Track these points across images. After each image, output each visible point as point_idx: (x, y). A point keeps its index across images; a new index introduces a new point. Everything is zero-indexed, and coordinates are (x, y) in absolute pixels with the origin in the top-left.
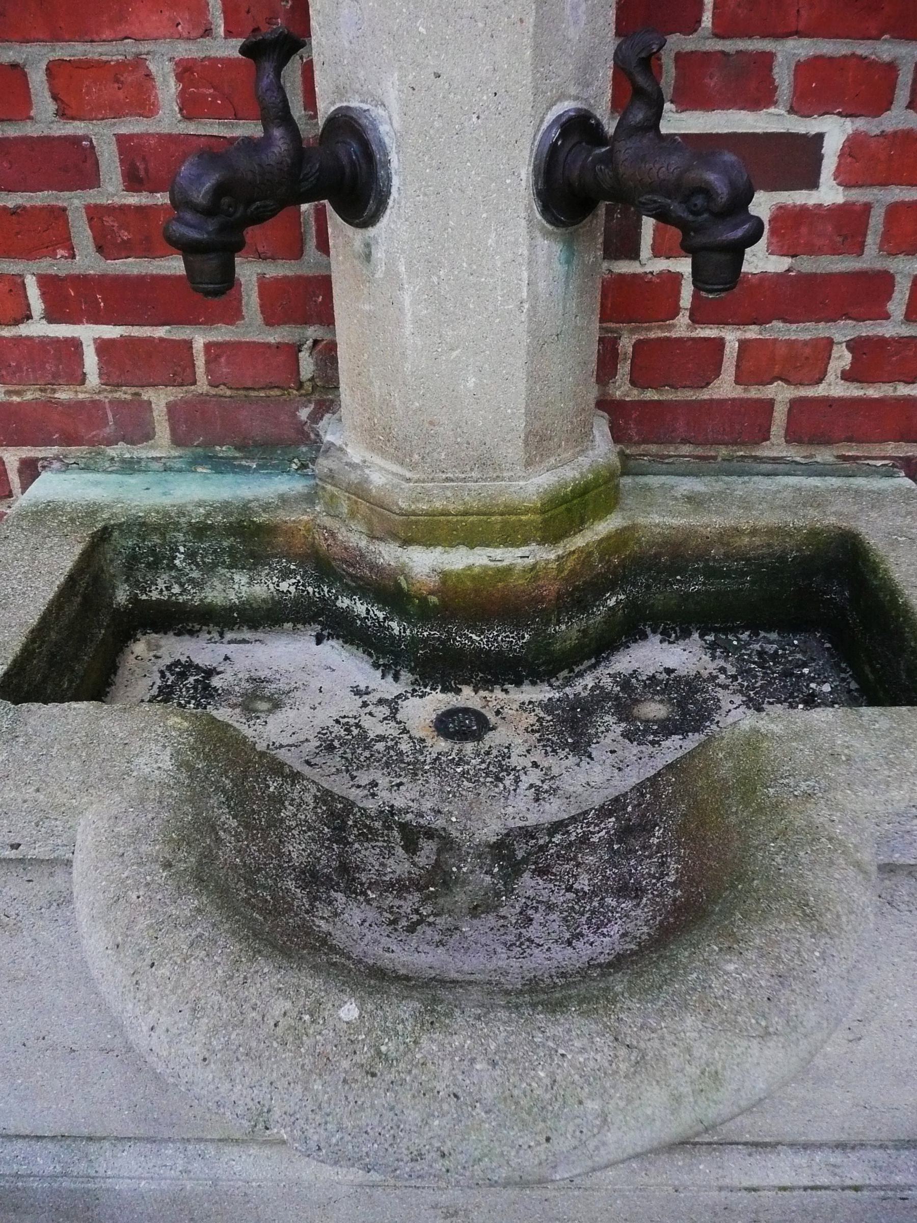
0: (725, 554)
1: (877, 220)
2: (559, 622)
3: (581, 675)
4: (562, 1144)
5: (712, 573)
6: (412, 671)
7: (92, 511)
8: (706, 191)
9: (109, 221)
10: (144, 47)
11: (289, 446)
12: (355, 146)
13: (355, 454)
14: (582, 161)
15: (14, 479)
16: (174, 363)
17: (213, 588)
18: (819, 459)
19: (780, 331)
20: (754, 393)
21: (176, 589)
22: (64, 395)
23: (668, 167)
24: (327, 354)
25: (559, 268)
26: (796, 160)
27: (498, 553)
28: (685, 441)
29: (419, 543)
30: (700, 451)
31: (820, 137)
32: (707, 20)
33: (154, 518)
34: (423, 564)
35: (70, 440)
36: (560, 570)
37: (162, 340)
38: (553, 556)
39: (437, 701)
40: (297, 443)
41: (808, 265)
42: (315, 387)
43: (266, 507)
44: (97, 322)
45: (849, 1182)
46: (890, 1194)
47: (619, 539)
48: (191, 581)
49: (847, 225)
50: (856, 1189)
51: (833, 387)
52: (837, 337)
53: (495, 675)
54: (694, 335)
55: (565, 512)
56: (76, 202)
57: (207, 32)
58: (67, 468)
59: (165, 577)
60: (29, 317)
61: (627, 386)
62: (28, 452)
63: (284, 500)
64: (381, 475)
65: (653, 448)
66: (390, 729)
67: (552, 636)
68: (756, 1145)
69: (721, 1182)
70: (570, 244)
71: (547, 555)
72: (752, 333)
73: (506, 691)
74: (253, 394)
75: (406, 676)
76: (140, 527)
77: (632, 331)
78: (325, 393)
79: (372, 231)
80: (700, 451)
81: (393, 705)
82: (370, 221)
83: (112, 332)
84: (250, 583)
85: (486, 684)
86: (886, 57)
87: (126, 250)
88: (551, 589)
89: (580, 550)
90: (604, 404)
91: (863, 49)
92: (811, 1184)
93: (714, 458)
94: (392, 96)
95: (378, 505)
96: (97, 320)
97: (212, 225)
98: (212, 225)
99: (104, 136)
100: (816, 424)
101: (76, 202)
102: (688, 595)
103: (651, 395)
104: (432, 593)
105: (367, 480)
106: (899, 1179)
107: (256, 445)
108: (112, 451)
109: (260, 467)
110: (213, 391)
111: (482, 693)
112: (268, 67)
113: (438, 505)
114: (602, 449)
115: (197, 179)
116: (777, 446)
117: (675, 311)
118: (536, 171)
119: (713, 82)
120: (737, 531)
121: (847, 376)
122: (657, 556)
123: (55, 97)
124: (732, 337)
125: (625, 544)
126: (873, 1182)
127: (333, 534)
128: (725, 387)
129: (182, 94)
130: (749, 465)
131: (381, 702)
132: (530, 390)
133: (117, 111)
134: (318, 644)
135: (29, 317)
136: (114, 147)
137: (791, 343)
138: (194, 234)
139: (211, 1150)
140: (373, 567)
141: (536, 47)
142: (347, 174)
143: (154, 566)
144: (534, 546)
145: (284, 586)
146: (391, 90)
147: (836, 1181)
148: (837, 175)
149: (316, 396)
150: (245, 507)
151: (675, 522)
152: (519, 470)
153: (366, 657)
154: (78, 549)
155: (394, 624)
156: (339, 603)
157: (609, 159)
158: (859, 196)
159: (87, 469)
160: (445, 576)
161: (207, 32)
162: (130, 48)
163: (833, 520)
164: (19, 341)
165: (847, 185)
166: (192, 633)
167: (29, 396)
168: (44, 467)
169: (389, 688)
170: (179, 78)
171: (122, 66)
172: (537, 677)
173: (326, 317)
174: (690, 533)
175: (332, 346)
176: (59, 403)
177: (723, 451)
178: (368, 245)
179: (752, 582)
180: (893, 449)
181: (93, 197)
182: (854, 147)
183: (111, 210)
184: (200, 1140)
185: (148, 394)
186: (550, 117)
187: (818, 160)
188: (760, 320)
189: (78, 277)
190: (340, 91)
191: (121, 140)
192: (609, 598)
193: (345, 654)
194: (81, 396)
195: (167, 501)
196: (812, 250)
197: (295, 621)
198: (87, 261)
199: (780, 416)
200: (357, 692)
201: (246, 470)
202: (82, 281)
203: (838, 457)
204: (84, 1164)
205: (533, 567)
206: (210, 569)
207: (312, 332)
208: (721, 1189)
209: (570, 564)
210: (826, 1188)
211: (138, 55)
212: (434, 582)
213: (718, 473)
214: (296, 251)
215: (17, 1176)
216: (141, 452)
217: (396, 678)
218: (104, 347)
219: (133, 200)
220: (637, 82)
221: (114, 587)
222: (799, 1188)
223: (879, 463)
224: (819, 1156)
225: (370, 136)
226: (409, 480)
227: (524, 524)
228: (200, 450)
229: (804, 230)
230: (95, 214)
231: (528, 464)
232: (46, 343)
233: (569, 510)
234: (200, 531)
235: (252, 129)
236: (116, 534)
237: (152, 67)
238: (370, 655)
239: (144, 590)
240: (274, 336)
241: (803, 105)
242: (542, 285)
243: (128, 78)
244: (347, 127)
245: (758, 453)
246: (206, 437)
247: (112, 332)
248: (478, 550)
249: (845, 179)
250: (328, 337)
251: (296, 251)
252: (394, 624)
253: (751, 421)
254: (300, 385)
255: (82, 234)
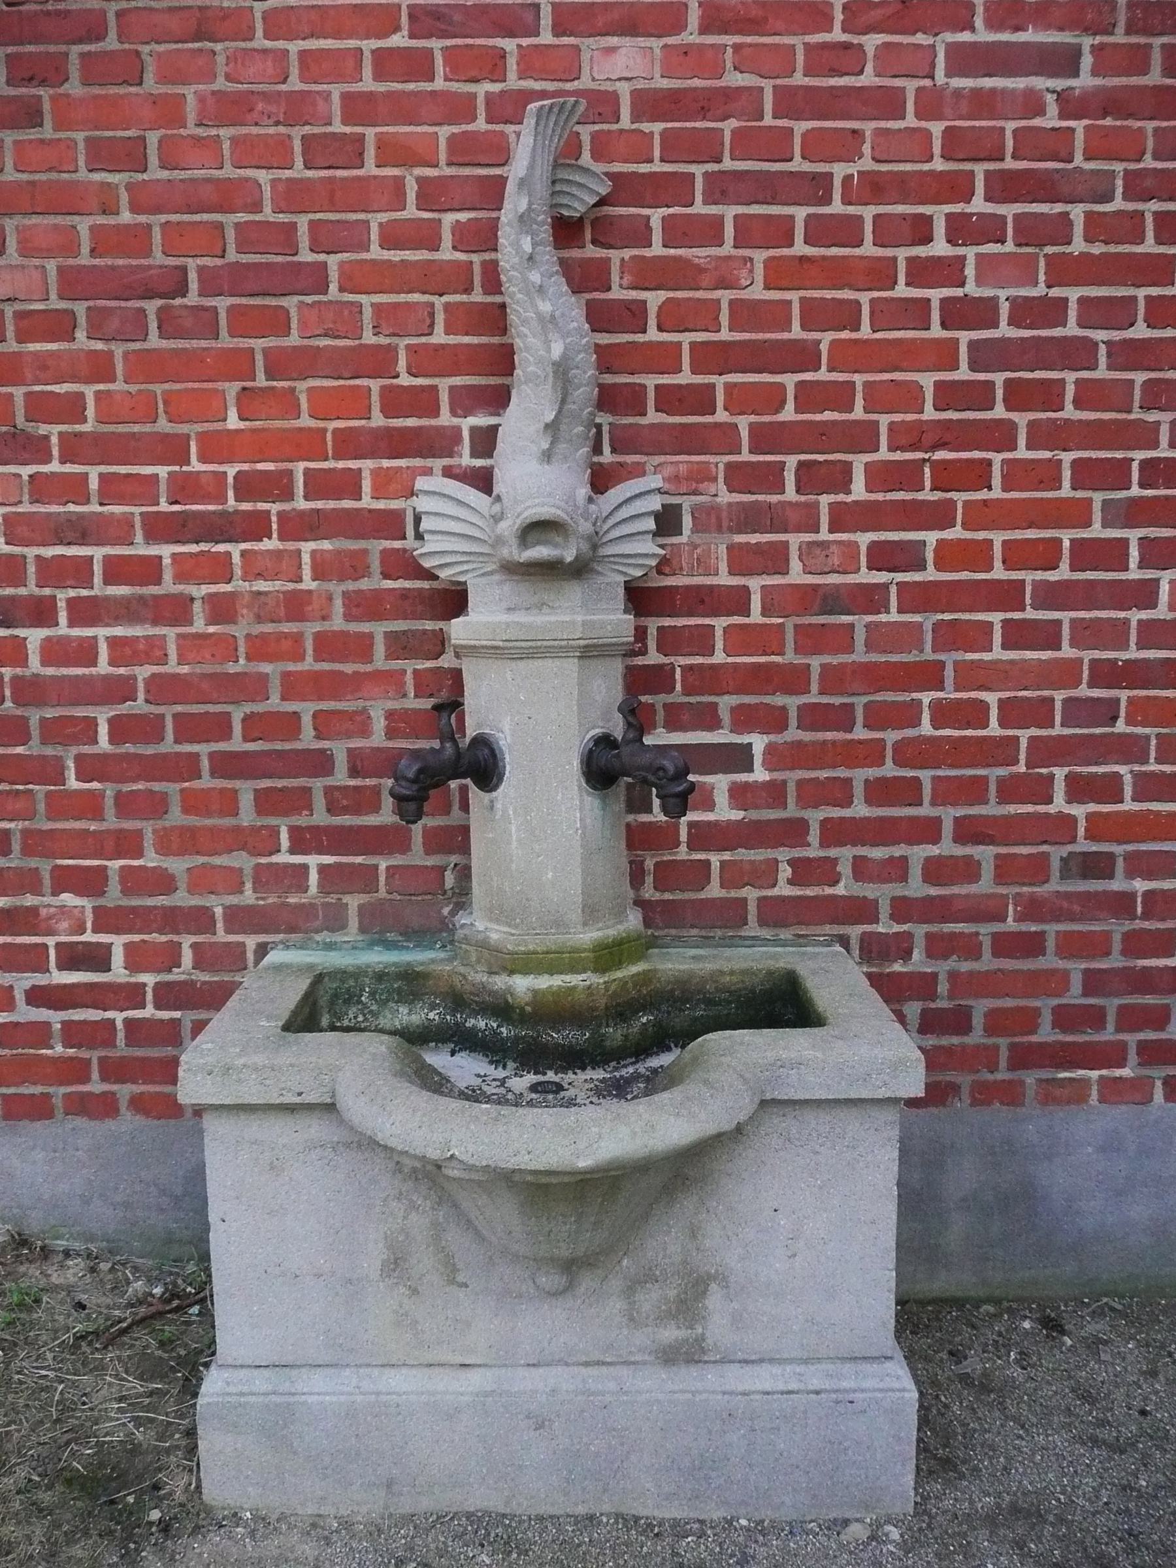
0: (716, 988)
1: (791, 789)
2: (608, 1026)
3: (625, 1066)
4: (582, 1145)
5: (709, 1002)
6: (515, 1061)
7: (311, 967)
8: (662, 768)
9: (337, 794)
10: (368, 703)
11: (437, 931)
12: (486, 751)
13: (480, 926)
14: (605, 758)
15: (250, 956)
16: (365, 879)
17: (385, 1017)
18: (782, 937)
19: (743, 854)
20: (733, 894)
21: (360, 1018)
22: (292, 900)
23: (645, 759)
24: (465, 873)
25: (598, 812)
26: (739, 758)
27: (568, 978)
28: (692, 926)
29: (520, 972)
30: (703, 933)
31: (750, 744)
32: (678, 687)
33: (351, 969)
34: (522, 985)
35: (292, 929)
36: (607, 990)
37: (360, 864)
38: (601, 981)
39: (531, 1078)
40: (441, 931)
41: (754, 815)
42: (454, 893)
43: (422, 964)
44: (320, 853)
45: (811, 1387)
46: (840, 1397)
47: (645, 978)
48: (371, 1012)
49: (775, 793)
50: (817, 1393)
51: (783, 889)
52: (780, 858)
53: (568, 1063)
54: (692, 857)
55: (608, 955)
56: (318, 785)
57: (405, 696)
58: (288, 947)
59: (354, 1009)
60: (279, 851)
61: (652, 891)
62: (262, 938)
63: (433, 961)
64: (496, 933)
65: (673, 932)
66: (502, 1090)
67: (604, 1035)
69: (723, 1388)
70: (604, 799)
72: (727, 856)
73: (575, 1073)
74: (413, 898)
75: (511, 1065)
76: (342, 974)
77: (653, 856)
78: (462, 897)
79: (494, 794)
80: (703, 933)
81: (503, 1082)
82: (494, 788)
83: (328, 860)
84: (409, 1014)
85: (563, 1070)
86: (780, 704)
87: (345, 811)
88: (602, 1002)
89: (620, 979)
90: (639, 903)
91: (767, 699)
92: (785, 1389)
93: (714, 937)
94: (506, 728)
95: (496, 950)
96: (320, 852)
97: (415, 787)
98: (415, 787)
99: (339, 749)
100: (776, 913)
101: (319, 784)
102: (696, 1019)
103: (667, 896)
104: (527, 1004)
105: (488, 937)
106: (845, 1384)
107: (415, 932)
108: (318, 937)
109: (415, 946)
110: (389, 897)
111: (560, 1075)
112: (445, 715)
113: (531, 947)
114: (633, 920)
115: (409, 766)
116: (753, 929)
117: (677, 844)
118: (582, 762)
119: (685, 718)
120: (722, 973)
121: (791, 882)
122: (673, 991)
123: (315, 729)
124: (715, 859)
125: (650, 980)
126: (827, 1387)
127: (464, 977)
128: (714, 890)
129: (387, 727)
130: (738, 941)
131: (494, 1080)
132: (584, 880)
133: (349, 735)
134: (452, 1055)
135: (279, 851)
136: (345, 754)
137: (752, 862)
138: (405, 792)
139: (376, 1371)
140: (492, 993)
141: (579, 705)
142: (484, 766)
143: (347, 1002)
144: (589, 973)
145: (431, 1016)
146: (506, 724)
147: (802, 1387)
148: (764, 764)
149: (454, 900)
150: (409, 963)
151: (682, 967)
152: (580, 928)
153: (485, 1059)
154: (309, 981)
155: (503, 1030)
156: (467, 1025)
157: (618, 756)
159: (301, 948)
160: (535, 992)
161: (405, 696)
162: (360, 704)
163: (782, 965)
164: (270, 865)
165: (770, 770)
167: (270, 901)
168: (272, 949)
169: (501, 1073)
170: (386, 718)
171: (355, 713)
172: (595, 1065)
173: (465, 849)
174: (691, 974)
175: (468, 868)
176: (289, 905)
177: (719, 933)
178: (492, 801)
179: (737, 1008)
180: (828, 929)
181: (329, 781)
182: (770, 750)
183: (338, 788)
184: (368, 1365)
185: (347, 899)
186: (588, 736)
188: (731, 848)
189: (313, 827)
190: (479, 725)
191: (349, 750)
192: (642, 1016)
193: (470, 1059)
194: (303, 900)
195: (358, 962)
196: (756, 807)
197: (437, 1041)
198: (320, 817)
199: (752, 908)
200: (478, 1076)
201: (407, 948)
202: (315, 830)
204: (287, 1384)
205: (589, 987)
206: (384, 1003)
207: (454, 859)
208: (724, 1393)
209: (613, 987)
210: (797, 1392)
211: (364, 707)
212: (528, 998)
213: (716, 946)
214: (447, 811)
215: (242, 1394)
216: (338, 937)
217: (504, 1067)
218: (323, 869)
219: (352, 782)
220: (637, 718)
222: (778, 1392)
224: (788, 1368)
225: (495, 747)
226: (513, 935)
227: (583, 959)
228: (376, 936)
229: (749, 795)
230: (328, 791)
231: (585, 924)
232: (287, 866)
233: (610, 953)
235: (436, 744)
236: (326, 979)
237: (372, 714)
238: (487, 1056)
239: (339, 1019)
240: (430, 861)
241: (737, 728)
242: (588, 821)
243: (359, 719)
244: (482, 742)
245: (743, 934)
246: (379, 925)
247: (328, 860)
248: (555, 977)
249: (769, 766)
250: (465, 861)
251: (447, 811)
252: (503, 1030)
253: (733, 913)
254: (445, 892)
255: (319, 802)
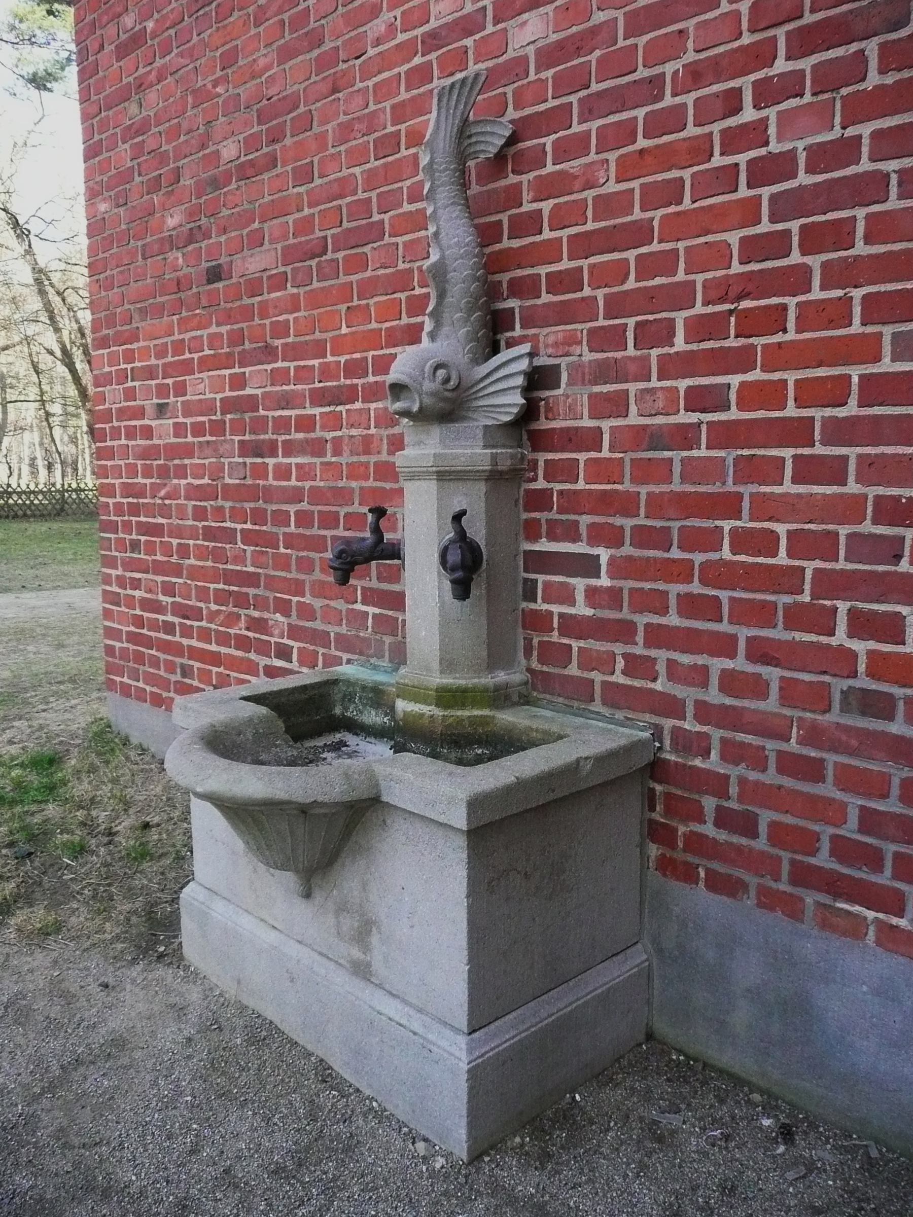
10: (396, 510)
20: (586, 675)
28: (559, 695)
30: (566, 702)
31: (598, 556)
38: (441, 714)
45: (412, 1028)
49: (613, 597)
65: (548, 697)
68: (391, 993)
71: (439, 712)
77: (537, 636)
80: (566, 702)
86: (618, 524)
89: (458, 717)
91: (610, 520)
103: (545, 669)
116: (597, 706)
122: (503, 735)
125: (488, 724)
132: (441, 641)
158: (618, 583)
165: (612, 578)
166: (357, 735)
182: (612, 561)
187: (599, 566)
196: (602, 607)
203: (625, 717)
206: (365, 705)
221: (335, 706)
223: (642, 724)
229: (597, 596)
233: (454, 696)
234: (364, 688)
241: (592, 542)
